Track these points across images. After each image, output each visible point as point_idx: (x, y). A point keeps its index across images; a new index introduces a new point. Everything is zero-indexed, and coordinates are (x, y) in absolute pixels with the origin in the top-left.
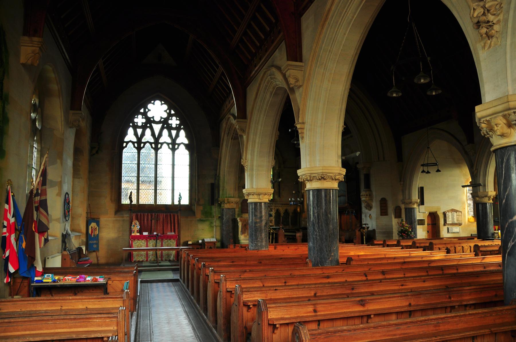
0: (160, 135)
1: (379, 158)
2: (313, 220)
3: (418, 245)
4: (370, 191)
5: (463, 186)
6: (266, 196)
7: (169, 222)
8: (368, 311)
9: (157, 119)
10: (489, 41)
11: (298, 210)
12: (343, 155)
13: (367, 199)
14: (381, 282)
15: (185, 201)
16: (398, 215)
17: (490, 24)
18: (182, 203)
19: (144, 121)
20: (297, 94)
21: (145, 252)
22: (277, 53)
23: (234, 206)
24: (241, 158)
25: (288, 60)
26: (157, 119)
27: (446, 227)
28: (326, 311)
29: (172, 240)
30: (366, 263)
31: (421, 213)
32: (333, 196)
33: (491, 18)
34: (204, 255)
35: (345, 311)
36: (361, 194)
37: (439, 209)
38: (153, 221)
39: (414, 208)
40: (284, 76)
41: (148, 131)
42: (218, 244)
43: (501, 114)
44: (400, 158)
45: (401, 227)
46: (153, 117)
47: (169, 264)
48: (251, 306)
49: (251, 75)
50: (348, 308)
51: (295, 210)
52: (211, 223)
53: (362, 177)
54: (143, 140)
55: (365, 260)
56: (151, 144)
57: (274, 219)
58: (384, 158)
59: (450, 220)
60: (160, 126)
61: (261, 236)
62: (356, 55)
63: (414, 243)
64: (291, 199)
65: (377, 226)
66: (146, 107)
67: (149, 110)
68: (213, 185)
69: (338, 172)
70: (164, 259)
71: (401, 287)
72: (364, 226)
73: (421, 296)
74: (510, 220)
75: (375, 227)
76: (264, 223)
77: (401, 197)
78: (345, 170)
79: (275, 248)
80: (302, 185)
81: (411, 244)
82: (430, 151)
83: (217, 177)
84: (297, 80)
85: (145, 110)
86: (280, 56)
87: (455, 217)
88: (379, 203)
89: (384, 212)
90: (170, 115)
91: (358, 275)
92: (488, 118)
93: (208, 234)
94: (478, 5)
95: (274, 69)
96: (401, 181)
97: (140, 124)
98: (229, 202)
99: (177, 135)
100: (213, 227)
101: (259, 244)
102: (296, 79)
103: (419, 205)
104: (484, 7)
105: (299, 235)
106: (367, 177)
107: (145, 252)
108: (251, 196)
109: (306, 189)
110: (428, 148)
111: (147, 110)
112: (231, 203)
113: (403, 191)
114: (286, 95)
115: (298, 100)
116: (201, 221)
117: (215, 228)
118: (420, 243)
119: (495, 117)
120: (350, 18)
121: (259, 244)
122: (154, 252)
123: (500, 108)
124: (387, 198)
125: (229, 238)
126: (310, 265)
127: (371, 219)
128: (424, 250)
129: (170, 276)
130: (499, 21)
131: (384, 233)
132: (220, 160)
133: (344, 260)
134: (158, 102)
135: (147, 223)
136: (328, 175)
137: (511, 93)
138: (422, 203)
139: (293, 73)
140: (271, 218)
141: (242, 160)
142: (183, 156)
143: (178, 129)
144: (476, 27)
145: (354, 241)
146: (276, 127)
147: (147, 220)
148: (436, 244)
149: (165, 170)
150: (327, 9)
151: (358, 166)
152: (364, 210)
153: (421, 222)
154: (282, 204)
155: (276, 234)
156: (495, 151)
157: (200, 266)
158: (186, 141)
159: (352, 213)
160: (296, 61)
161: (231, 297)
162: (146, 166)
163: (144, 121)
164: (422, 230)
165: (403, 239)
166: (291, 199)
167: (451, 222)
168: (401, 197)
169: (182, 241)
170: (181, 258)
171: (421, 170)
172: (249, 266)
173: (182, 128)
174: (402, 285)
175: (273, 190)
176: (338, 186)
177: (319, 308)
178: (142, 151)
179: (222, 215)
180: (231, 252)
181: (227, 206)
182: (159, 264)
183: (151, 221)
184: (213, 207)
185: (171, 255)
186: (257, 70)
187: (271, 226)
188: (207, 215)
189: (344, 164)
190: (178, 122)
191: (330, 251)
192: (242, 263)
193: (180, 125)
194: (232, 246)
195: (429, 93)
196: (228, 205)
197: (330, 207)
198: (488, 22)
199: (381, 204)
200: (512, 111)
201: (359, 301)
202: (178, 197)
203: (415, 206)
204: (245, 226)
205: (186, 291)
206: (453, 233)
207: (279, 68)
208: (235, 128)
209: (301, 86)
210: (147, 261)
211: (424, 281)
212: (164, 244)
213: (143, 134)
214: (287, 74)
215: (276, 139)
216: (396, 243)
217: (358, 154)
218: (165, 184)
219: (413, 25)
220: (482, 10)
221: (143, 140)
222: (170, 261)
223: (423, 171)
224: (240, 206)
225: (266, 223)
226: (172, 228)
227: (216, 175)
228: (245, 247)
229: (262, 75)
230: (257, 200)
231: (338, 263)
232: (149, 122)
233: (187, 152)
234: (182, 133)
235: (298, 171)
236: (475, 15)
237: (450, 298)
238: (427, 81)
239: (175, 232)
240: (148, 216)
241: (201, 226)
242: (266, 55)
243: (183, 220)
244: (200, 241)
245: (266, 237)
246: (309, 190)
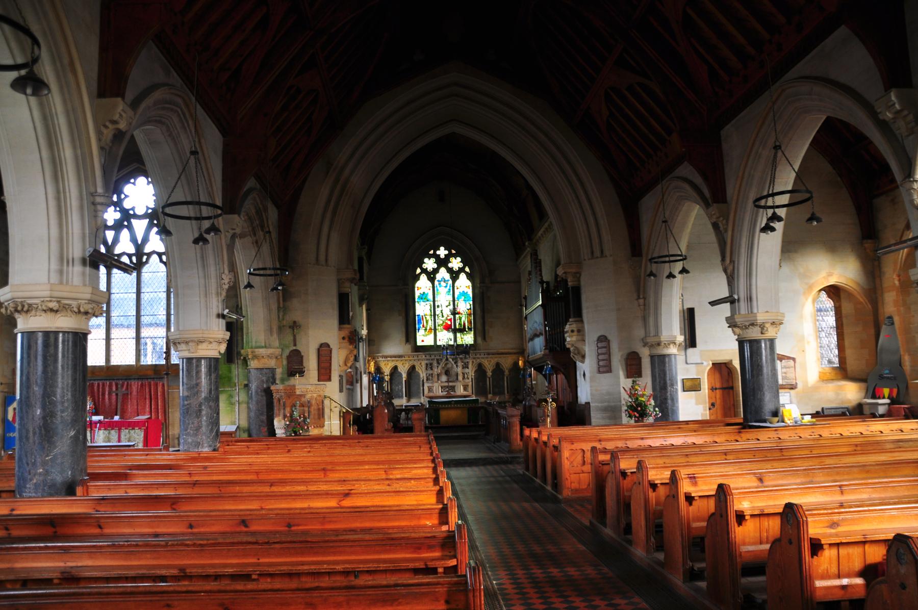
0: (146, 239)
1: (592, 253)
4: (582, 321)
5: (713, 303)
7: (148, 396)
9: (140, 211)
11: (520, 363)
16: (633, 367)
23: (272, 363)
26: (140, 211)
29: (137, 430)
41: (125, 233)
44: (636, 249)
46: (133, 209)
51: (516, 364)
52: (231, 396)
54: (147, 250)
58: (602, 252)
65: (592, 394)
66: (119, 192)
75: (589, 400)
77: (640, 333)
85: (119, 197)
89: (605, 367)
96: (639, 298)
97: (110, 223)
98: (255, 357)
100: (232, 404)
103: (686, 349)
113: (645, 319)
131: (605, 409)
135: (110, 399)
138: (691, 342)
140: (467, 381)
147: (110, 394)
163: (118, 215)
164: (693, 401)
175: (229, 334)
184: (233, 366)
196: (256, 361)
224: (285, 362)
232: (127, 217)
240: (110, 386)
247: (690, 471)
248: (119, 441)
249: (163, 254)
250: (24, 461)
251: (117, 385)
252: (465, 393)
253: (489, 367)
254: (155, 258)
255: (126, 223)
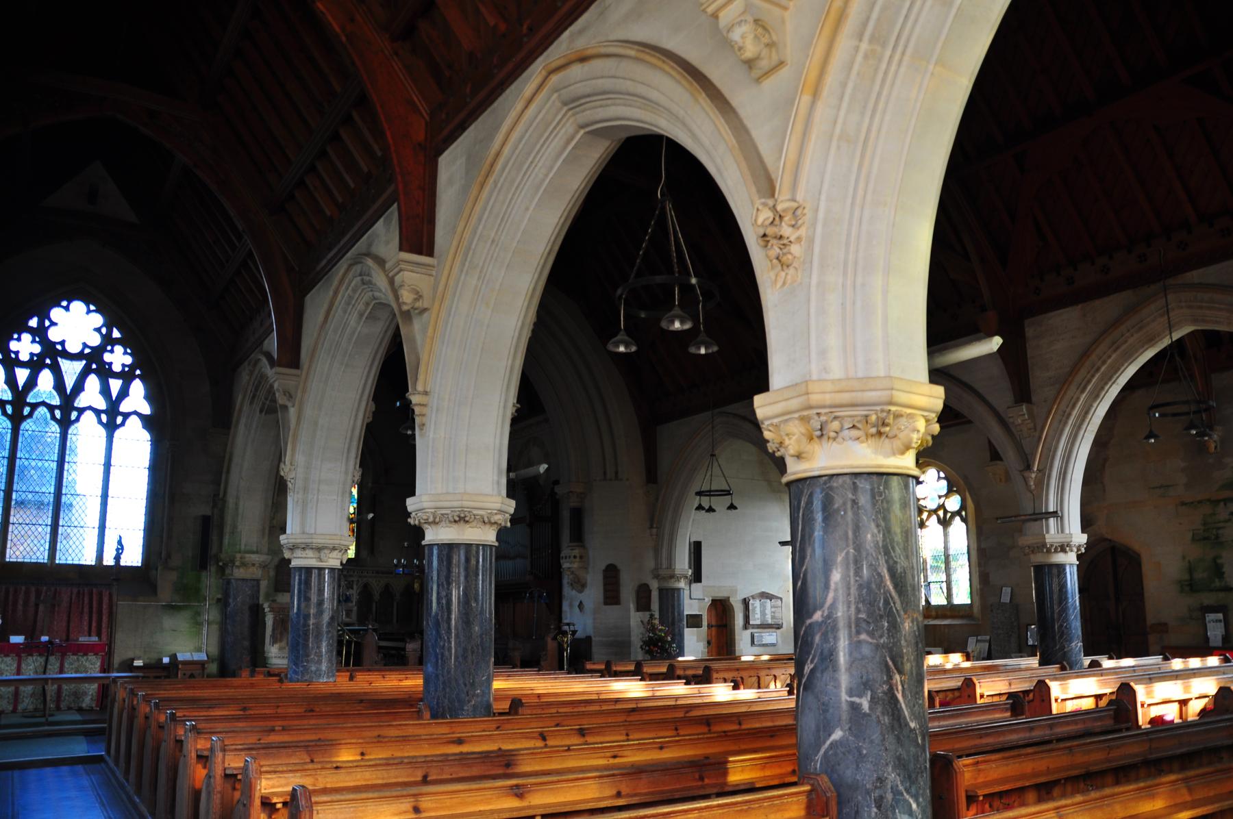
0: (79, 387)
1: (605, 473)
2: (437, 614)
3: (679, 672)
4: (583, 547)
6: (335, 554)
7: (86, 610)
8: (529, 807)
9: (73, 348)
10: (783, 274)
11: (416, 586)
12: (509, 470)
13: (575, 565)
14: (569, 750)
15: (133, 557)
16: (643, 603)
17: (785, 241)
18: (123, 563)
19: (37, 349)
20: (417, 325)
21: (12, 689)
22: (380, 224)
23: (256, 573)
24: (280, 460)
25: (401, 249)
26: (73, 348)
27: (748, 632)
28: (442, 808)
29: (92, 657)
30: (554, 711)
31: (694, 601)
32: (481, 561)
33: (786, 230)
34: (173, 694)
35: (482, 808)
36: (562, 554)
37: (735, 591)
38: (41, 608)
39: (679, 589)
40: (391, 282)
41: (46, 379)
42: (213, 668)
43: (796, 415)
44: (651, 475)
45: (649, 631)
47: (78, 717)
48: (279, 806)
49: (318, 268)
50: (489, 804)
51: (409, 587)
52: (198, 614)
53: (566, 515)
55: (550, 704)
56: (51, 408)
57: (355, 608)
58: (617, 473)
59: (758, 616)
60: (79, 366)
61: (319, 647)
62: (549, 254)
63: (672, 668)
64: (399, 561)
66: (44, 315)
67: (53, 324)
68: (206, 521)
69: (498, 506)
70: (63, 705)
71: (612, 761)
72: (566, 628)
73: (644, 776)
74: (808, 622)
75: (590, 631)
76: (326, 617)
78: (513, 503)
79: (351, 678)
80: (419, 532)
81: (665, 670)
82: (715, 464)
83: (218, 500)
84: (419, 297)
85: (41, 323)
86: (384, 235)
87: (768, 611)
88: (600, 577)
89: (612, 596)
90: (108, 341)
91: (527, 737)
92: (775, 421)
93: (186, 642)
94: (765, 205)
95: (370, 262)
96: (651, 527)
98: (244, 565)
99: (124, 393)
100: (201, 624)
101: (313, 668)
102: (417, 293)
104: (774, 208)
105: (411, 647)
106: (578, 516)
107: (12, 689)
108: (298, 553)
109: (423, 543)
110: (713, 455)
111: (47, 323)
112: (250, 566)
113: (657, 551)
114: (393, 326)
115: (418, 338)
116: (172, 608)
117: (205, 628)
118: (685, 669)
119: (786, 421)
120: (541, 176)
121: (313, 668)
122: (39, 688)
123: (794, 404)
124: (620, 566)
125: (240, 653)
126: (427, 714)
127: (583, 612)
128: (686, 684)
129: (80, 748)
130: (799, 239)
132: (230, 460)
133: (505, 705)
134: (78, 306)
136: (475, 512)
137: (815, 377)
138: (697, 577)
139: (409, 278)
141: (282, 465)
142: (135, 444)
143: (127, 376)
144: (762, 243)
145: (542, 663)
146: (367, 392)
147: (26, 603)
148: (717, 671)
149: (84, 476)
150: (493, 151)
151: (557, 489)
152: (567, 591)
153: (695, 621)
154: (377, 572)
155: (358, 644)
156: (789, 484)
157: (162, 718)
158: (146, 409)
159: (540, 596)
160: (420, 253)
161: (234, 789)
162: (33, 464)
163: (37, 349)
164: (695, 638)
165: (653, 658)
166: (399, 561)
167: (758, 622)
168: (650, 564)
169: (117, 660)
170: (114, 700)
171: (696, 505)
172: (284, 718)
173: (138, 376)
174: (615, 757)
176: (498, 539)
177: (425, 803)
178: (25, 425)
179: (226, 594)
180: (243, 684)
181: (239, 573)
182: (51, 719)
183: (37, 605)
184: (204, 574)
185: (85, 694)
186: (333, 258)
187: (348, 625)
188: (188, 596)
189: (513, 490)
190: (128, 360)
191: (473, 684)
192: (267, 711)
193: (132, 367)
194: (245, 673)
195: (693, 350)
196: (242, 570)
197: (477, 585)
198: (781, 237)
199: (605, 577)
200: (815, 411)
201: (511, 787)
202: (115, 545)
203: (682, 584)
204: (282, 623)
205: (122, 787)
206: (764, 645)
207: (381, 262)
208: (272, 386)
209: (425, 310)
210: (14, 710)
211: (661, 748)
212: (66, 665)
213: (32, 383)
214: (398, 279)
215: (367, 421)
216: (632, 668)
217: (543, 468)
218: (83, 511)
219: (669, 206)
220: (770, 215)
221: (31, 399)
222: (80, 710)
223: (700, 508)
224: (272, 573)
225: (332, 618)
226: (94, 624)
227: (216, 495)
228: (280, 676)
229: (342, 271)
230: (313, 563)
231: (488, 711)
232: (51, 354)
233: (145, 436)
234: (137, 388)
235: (411, 504)
236: (760, 221)
237: (701, 779)
238: (687, 326)
239: (99, 634)
240: (27, 593)
241: (168, 622)
242: (356, 228)
243: (123, 606)
244: (166, 660)
245: (331, 651)
246: (431, 546)
247: (202, 744)
248: (18, 673)
249: (103, 411)
250: (461, 682)
251: (38, 593)
252: (348, 620)
253: (377, 586)
254: (89, 415)
255: (48, 361)
